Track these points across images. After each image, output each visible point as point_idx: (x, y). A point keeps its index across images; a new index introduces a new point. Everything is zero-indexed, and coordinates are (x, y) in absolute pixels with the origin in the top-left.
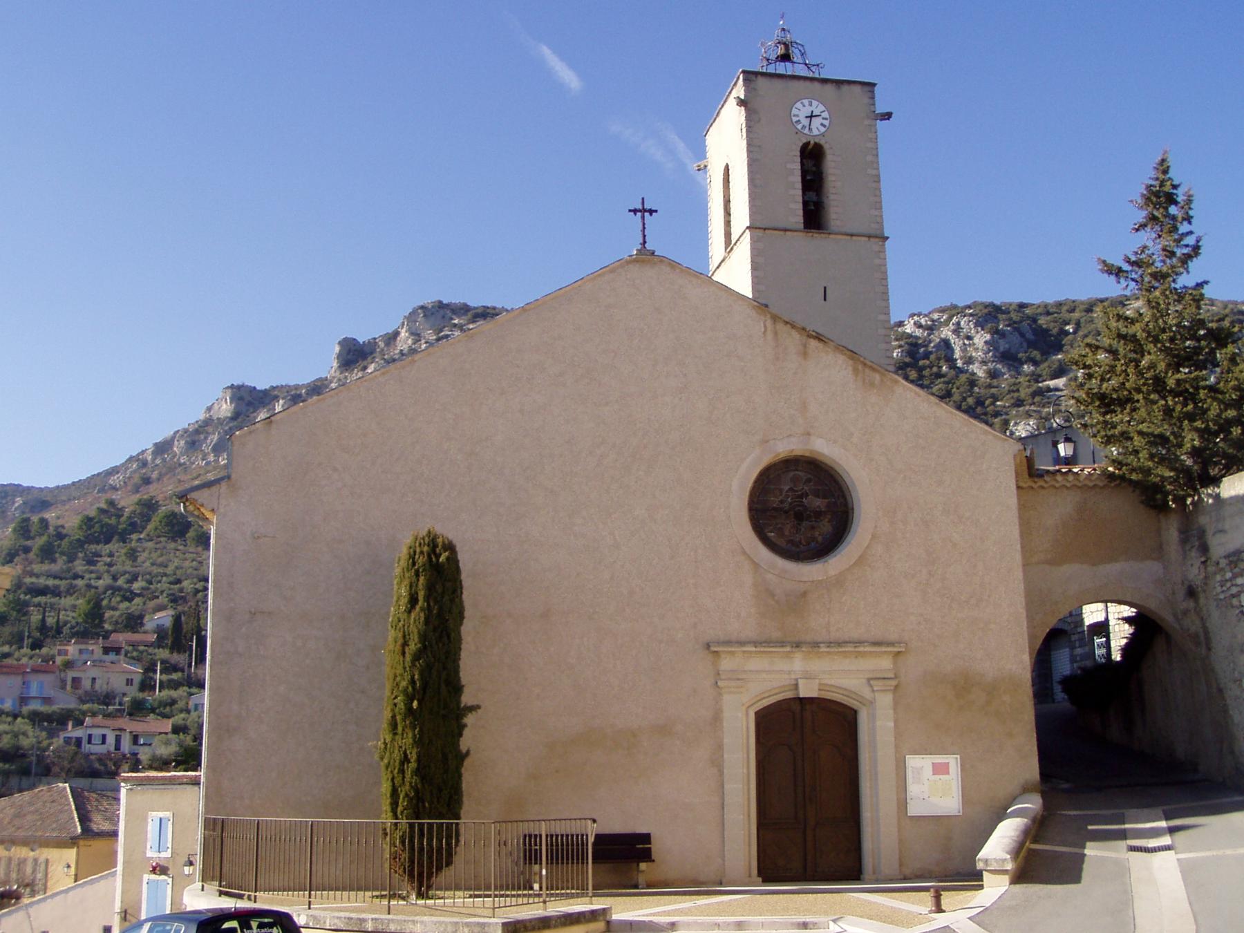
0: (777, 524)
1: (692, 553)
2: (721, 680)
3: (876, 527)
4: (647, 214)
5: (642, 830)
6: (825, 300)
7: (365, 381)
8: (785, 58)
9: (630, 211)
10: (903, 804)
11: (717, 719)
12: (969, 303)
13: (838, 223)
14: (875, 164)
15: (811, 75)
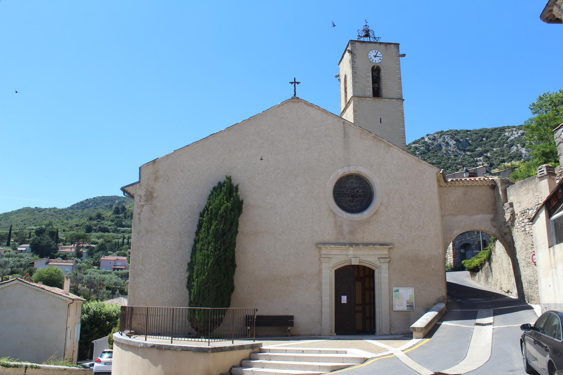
0: (345, 199)
1: (311, 210)
2: (322, 258)
3: (382, 200)
4: (296, 84)
5: (291, 314)
6: (381, 123)
7: (190, 146)
8: (367, 35)
9: (290, 83)
10: (391, 306)
11: (320, 272)
12: (448, 130)
13: (386, 95)
14: (399, 73)
15: (375, 41)
